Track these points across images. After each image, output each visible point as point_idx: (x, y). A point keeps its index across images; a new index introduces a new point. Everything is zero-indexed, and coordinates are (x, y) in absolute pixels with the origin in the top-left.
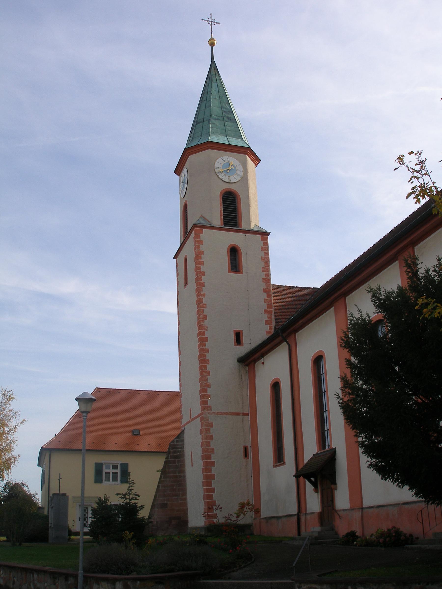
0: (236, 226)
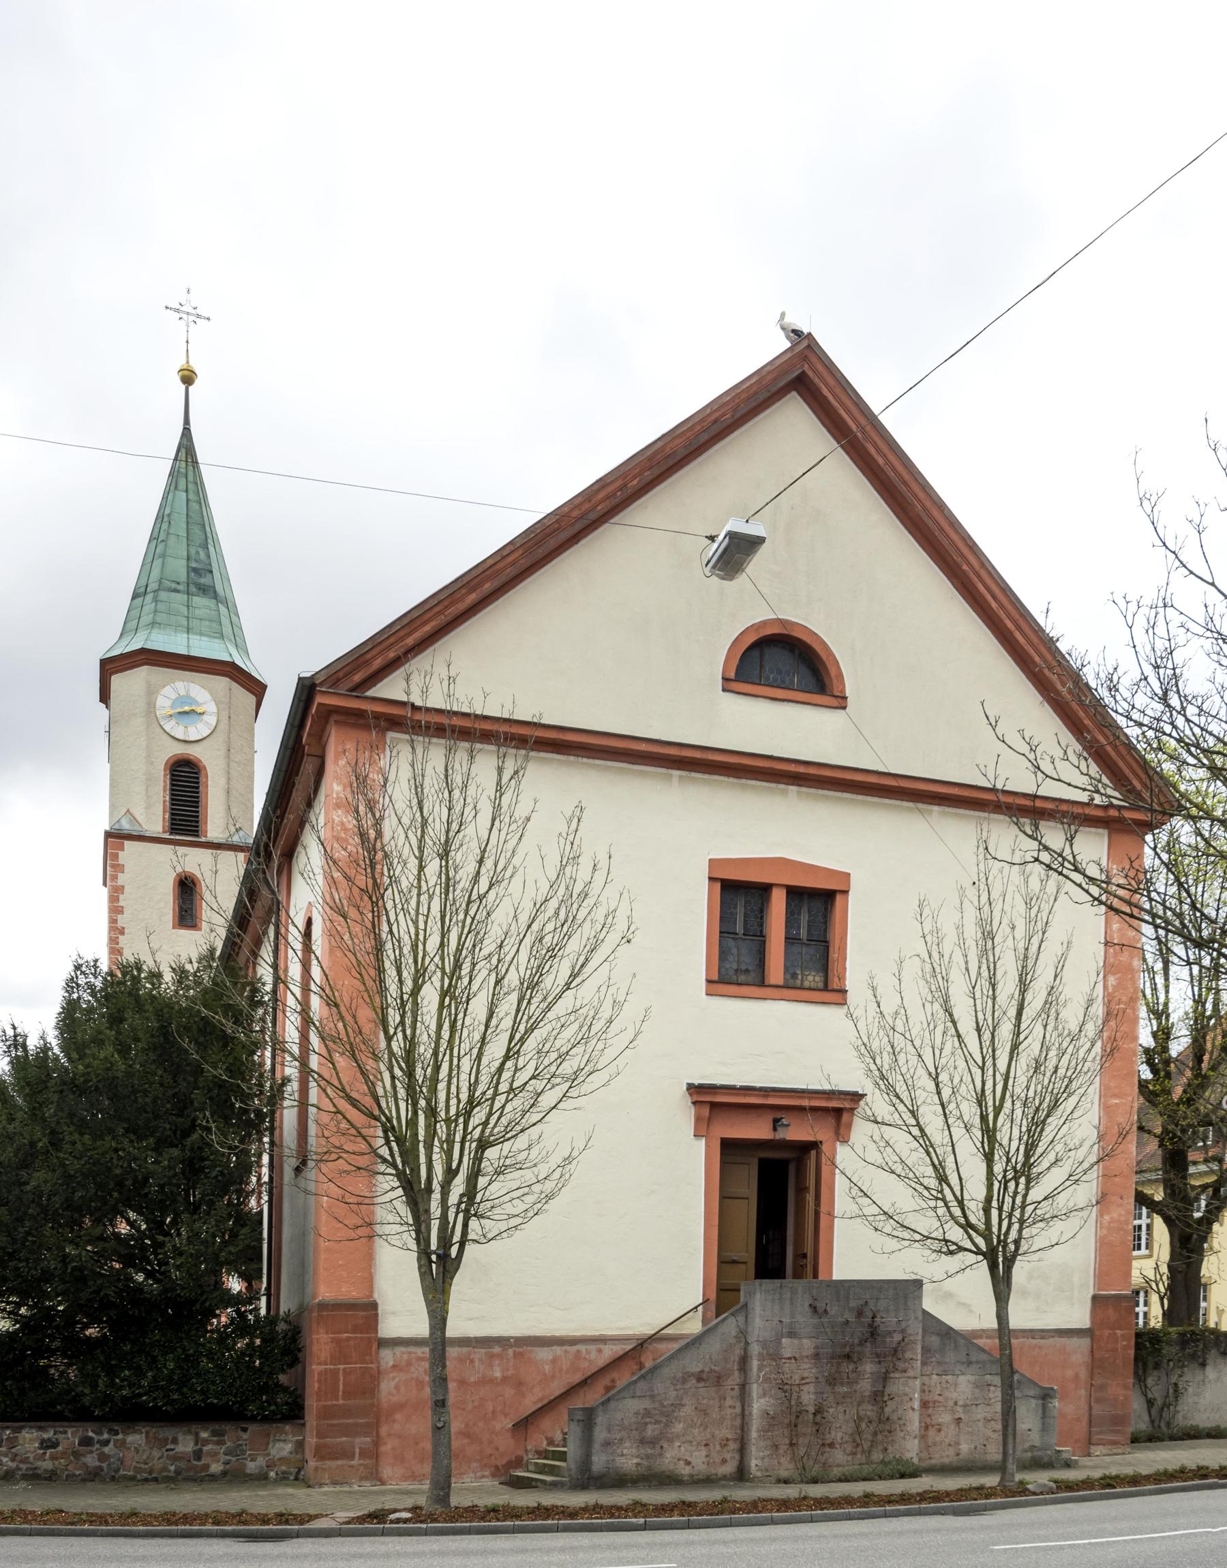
0: (195, 833)
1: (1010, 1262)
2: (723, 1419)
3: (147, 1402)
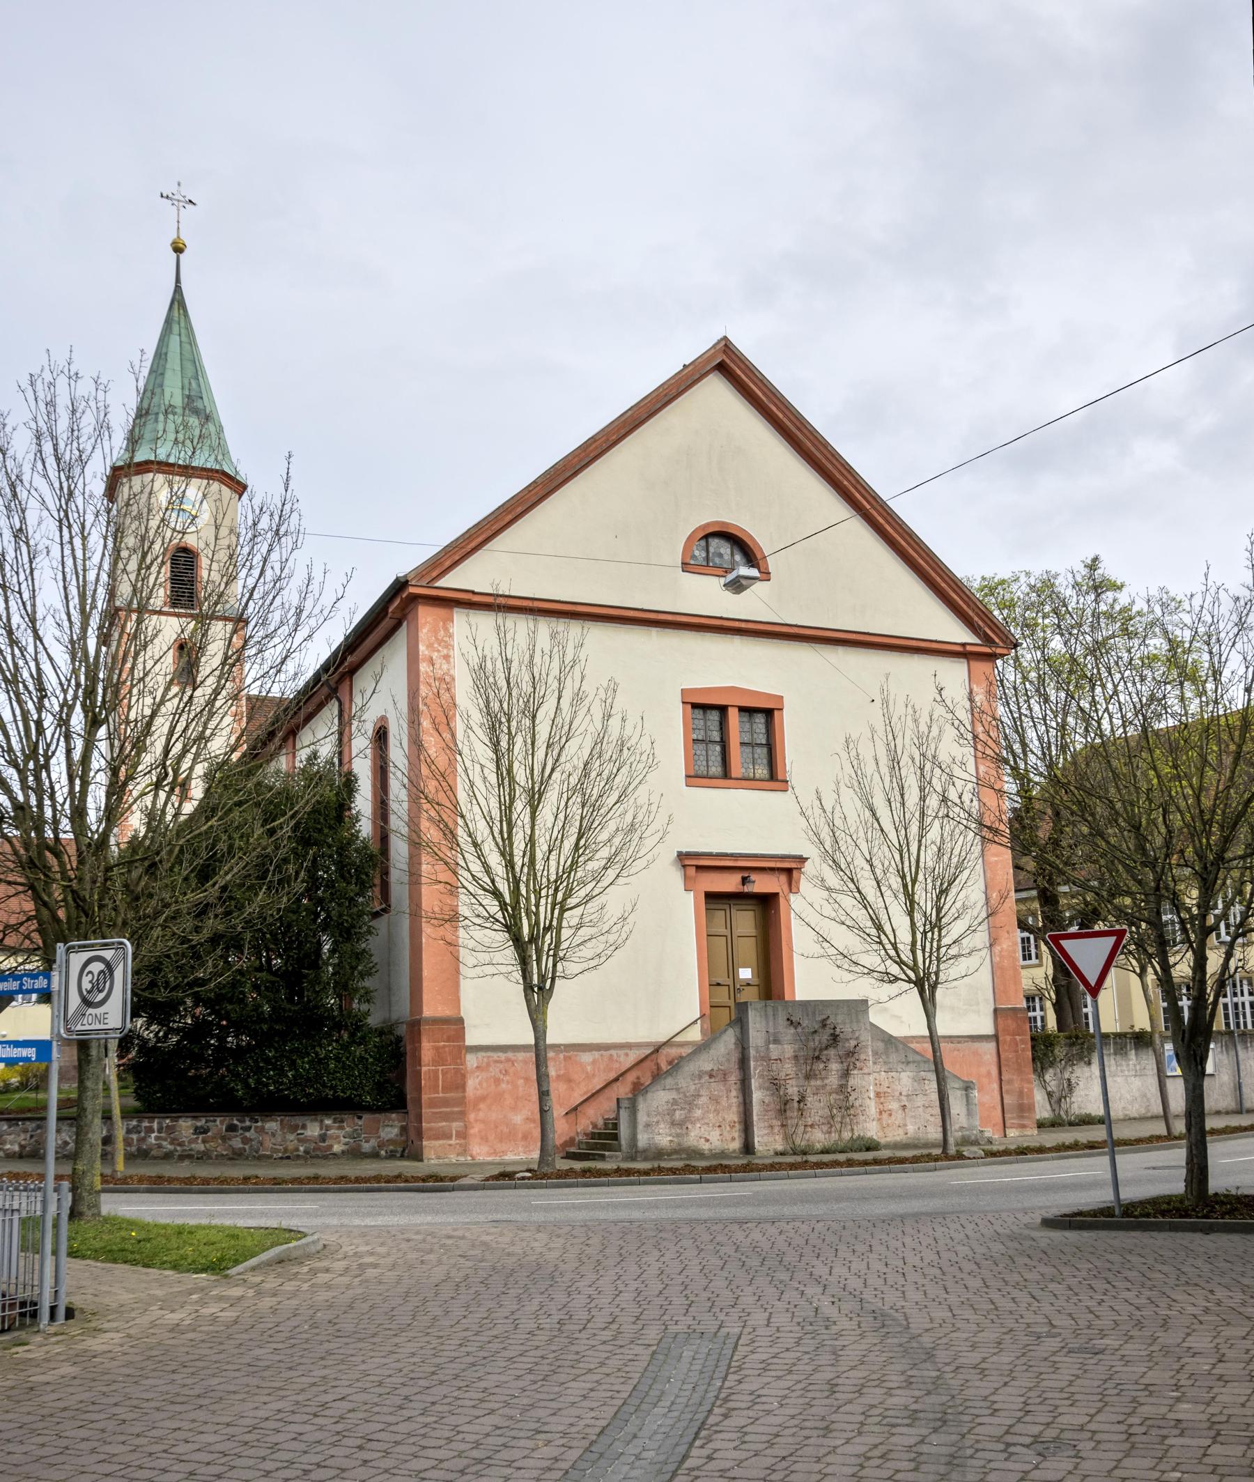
1: (933, 988)
2: (730, 1106)
3: (288, 1096)
